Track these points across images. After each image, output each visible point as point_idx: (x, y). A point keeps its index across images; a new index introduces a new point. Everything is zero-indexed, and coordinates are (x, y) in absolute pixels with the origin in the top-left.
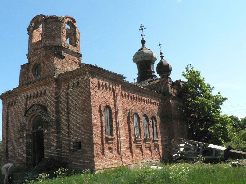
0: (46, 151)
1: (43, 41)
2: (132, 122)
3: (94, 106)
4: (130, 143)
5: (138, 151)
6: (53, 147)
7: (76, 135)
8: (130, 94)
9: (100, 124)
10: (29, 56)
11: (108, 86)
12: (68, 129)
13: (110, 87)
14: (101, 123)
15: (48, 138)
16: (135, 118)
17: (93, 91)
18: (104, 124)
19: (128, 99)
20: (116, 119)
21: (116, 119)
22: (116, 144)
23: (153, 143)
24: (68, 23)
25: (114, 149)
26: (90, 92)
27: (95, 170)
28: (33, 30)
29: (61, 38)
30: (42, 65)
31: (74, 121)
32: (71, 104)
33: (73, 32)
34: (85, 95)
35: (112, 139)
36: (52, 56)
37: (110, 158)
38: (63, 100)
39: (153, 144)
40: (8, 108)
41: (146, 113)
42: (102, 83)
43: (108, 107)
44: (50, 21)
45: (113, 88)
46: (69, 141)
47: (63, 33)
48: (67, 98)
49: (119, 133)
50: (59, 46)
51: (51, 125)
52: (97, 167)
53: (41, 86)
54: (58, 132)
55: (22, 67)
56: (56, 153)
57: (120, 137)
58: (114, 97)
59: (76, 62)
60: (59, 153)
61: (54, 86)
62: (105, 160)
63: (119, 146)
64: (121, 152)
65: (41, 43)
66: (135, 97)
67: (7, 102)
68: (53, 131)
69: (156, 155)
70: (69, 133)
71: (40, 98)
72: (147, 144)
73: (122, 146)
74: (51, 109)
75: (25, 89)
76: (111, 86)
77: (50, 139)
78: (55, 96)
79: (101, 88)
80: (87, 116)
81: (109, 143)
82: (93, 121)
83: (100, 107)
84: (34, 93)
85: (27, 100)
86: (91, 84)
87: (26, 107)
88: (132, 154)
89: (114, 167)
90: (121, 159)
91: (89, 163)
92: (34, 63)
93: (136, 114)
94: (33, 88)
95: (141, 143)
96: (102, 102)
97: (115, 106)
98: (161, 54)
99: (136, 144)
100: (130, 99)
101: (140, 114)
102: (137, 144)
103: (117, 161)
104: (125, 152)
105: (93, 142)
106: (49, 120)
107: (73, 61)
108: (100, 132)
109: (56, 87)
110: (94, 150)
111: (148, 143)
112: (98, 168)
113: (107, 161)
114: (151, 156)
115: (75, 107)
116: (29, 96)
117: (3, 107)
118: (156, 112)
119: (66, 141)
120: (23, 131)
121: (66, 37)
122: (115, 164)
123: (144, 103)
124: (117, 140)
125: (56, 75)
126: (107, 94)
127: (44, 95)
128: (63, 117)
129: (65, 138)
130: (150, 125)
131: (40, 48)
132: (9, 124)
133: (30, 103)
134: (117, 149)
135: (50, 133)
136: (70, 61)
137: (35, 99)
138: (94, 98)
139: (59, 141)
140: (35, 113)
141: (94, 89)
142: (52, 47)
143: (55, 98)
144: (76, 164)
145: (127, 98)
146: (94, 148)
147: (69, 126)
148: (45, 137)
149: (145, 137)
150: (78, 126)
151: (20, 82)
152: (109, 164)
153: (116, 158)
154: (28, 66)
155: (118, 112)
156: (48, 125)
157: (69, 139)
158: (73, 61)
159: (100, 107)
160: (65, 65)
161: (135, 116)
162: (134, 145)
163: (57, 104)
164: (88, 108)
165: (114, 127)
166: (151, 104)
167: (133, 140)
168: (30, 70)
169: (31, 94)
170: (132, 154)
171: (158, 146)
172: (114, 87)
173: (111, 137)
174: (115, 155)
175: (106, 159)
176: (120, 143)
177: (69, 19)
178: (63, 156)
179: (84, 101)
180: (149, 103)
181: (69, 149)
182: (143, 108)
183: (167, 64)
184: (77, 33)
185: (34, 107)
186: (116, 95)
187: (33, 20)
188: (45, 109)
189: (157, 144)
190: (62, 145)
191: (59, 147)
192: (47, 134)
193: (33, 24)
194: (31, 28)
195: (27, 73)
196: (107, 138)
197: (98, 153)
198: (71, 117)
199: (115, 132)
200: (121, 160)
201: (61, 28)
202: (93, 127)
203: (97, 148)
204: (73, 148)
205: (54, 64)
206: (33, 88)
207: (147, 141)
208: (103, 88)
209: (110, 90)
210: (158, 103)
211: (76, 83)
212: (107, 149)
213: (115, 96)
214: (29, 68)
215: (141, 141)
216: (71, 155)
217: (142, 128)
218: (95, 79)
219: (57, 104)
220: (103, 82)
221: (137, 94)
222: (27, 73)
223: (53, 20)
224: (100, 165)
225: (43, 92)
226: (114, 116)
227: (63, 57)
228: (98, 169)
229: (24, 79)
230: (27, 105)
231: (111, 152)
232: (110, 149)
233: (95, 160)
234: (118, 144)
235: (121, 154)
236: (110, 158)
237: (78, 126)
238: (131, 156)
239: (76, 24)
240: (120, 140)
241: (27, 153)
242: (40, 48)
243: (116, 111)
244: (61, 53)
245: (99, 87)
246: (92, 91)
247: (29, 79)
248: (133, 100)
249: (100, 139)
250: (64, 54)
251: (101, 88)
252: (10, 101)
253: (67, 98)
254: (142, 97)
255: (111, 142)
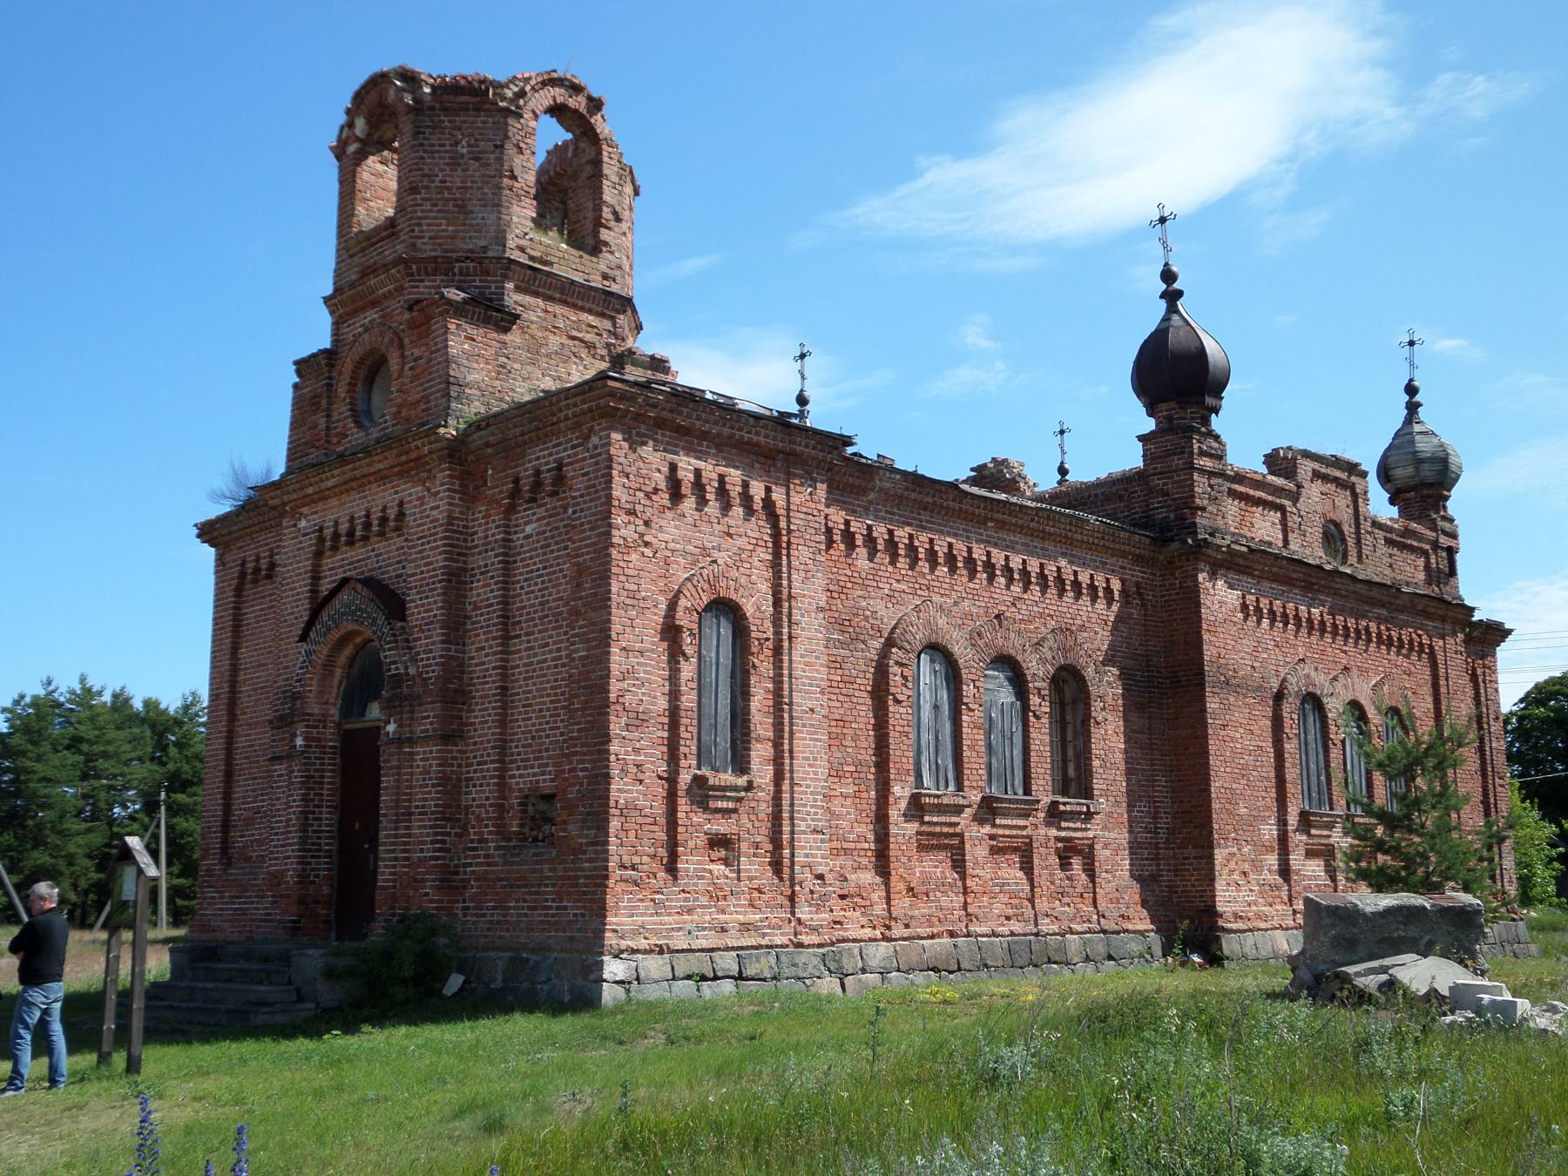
0: (387, 836)
1: (402, 225)
2: (899, 697)
3: (629, 601)
4: (881, 819)
5: (936, 867)
6: (420, 814)
7: (536, 759)
8: (902, 534)
9: (663, 703)
10: (342, 303)
11: (739, 489)
12: (503, 722)
13: (751, 498)
14: (674, 695)
15: (399, 767)
16: (927, 671)
17: (626, 518)
18: (688, 700)
19: (893, 562)
20: (777, 680)
21: (777, 680)
22: (762, 816)
23: (1048, 824)
24: (557, 111)
25: (744, 846)
26: (610, 525)
27: (602, 954)
28: (361, 156)
29: (499, 205)
30: (394, 363)
31: (532, 677)
32: (522, 588)
33: (588, 169)
34: (584, 539)
35: (736, 789)
36: (441, 314)
37: (717, 896)
38: (486, 561)
39: (1053, 832)
40: (239, 591)
41: (1012, 644)
42: (698, 473)
43: (725, 608)
44: (445, 109)
45: (774, 503)
46: (502, 786)
47: (514, 178)
48: (505, 554)
49: (792, 758)
50: (490, 254)
51: (419, 697)
52: (622, 938)
53: (382, 478)
54: (452, 734)
55: (304, 366)
56: (436, 850)
57: (792, 779)
58: (777, 554)
59: (590, 346)
60: (447, 850)
61: (442, 485)
62: (677, 901)
63: (786, 829)
64: (793, 863)
65: (393, 234)
66: (941, 549)
67: (234, 556)
68: (427, 731)
69: (1066, 900)
70: (503, 746)
71: (381, 546)
72: (1000, 832)
73: (804, 832)
74: (425, 607)
75: (310, 490)
76: (757, 490)
77: (412, 774)
78: (445, 538)
79: (689, 504)
80: (587, 657)
81: (717, 811)
82: (615, 687)
83: (672, 606)
84: (352, 519)
85: (319, 554)
86: (617, 480)
87: (314, 591)
88: (887, 884)
89: (731, 943)
90: (793, 906)
91: (583, 915)
92: (357, 352)
93: (937, 649)
94: (347, 487)
95: (954, 819)
96: (687, 579)
97: (777, 603)
98: (1168, 276)
99: (923, 823)
100: (903, 563)
101: (962, 652)
102: (924, 828)
103: (757, 917)
104: (820, 870)
105: (608, 798)
106: (412, 671)
107: (574, 338)
108: (665, 749)
109: (449, 490)
110: (607, 843)
111: (1004, 826)
112: (624, 944)
113: (690, 911)
114: (1031, 901)
115: (541, 604)
116: (328, 533)
117: (217, 584)
118: (1100, 639)
119: (488, 785)
120: (293, 722)
121: (535, 198)
122: (746, 927)
123: (1008, 587)
124: (774, 798)
125: (451, 421)
126: (729, 535)
127: (397, 529)
128: (482, 653)
129: (482, 771)
130: (1036, 716)
131: (386, 267)
132: (241, 677)
133: (336, 566)
134: (770, 847)
135: (411, 741)
136: (555, 341)
137: (359, 552)
138: (634, 557)
139: (451, 787)
140: (351, 627)
141: (639, 508)
142: (450, 261)
143: (445, 552)
144: (526, 915)
145: (883, 557)
146: (607, 835)
147: (504, 708)
148: (389, 758)
149: (995, 791)
150: (548, 710)
151: (295, 452)
152: (704, 929)
153: (756, 894)
154: (331, 366)
155: (790, 638)
156: (402, 700)
157: (502, 777)
158: (574, 338)
159: (672, 606)
160: (517, 366)
161: (932, 661)
162: (903, 830)
163: (456, 580)
164: (594, 610)
165: (761, 723)
166: (1062, 592)
167: (903, 805)
168: (342, 390)
169: (336, 523)
170: (887, 884)
171: (1091, 847)
172: (778, 496)
173: (728, 778)
174: (751, 879)
175: (686, 900)
176: (792, 812)
177: (558, 94)
178: (470, 865)
179: (580, 572)
180: (1044, 587)
181: (501, 831)
182: (998, 617)
183: (1193, 345)
184: (610, 170)
185: (344, 596)
186: (789, 543)
187: (358, 97)
188: (391, 602)
189: (1079, 835)
190: (467, 808)
191: (452, 812)
192: (399, 741)
193: (360, 125)
194: (352, 148)
195: (324, 403)
196: (699, 781)
197: (636, 860)
198: (520, 660)
199: (760, 754)
200: (793, 913)
201: (502, 147)
202: (612, 718)
203: (632, 834)
204: (521, 826)
205: (448, 362)
206: (347, 491)
207: (1006, 814)
208: (702, 502)
209: (749, 511)
210: (1116, 585)
211: (549, 471)
212: (701, 840)
213: (779, 546)
214: (334, 374)
215: (958, 810)
216: (506, 863)
217: (972, 736)
218: (647, 451)
219: (456, 580)
220: (701, 464)
221: (955, 535)
222: (324, 403)
223: (463, 98)
224: (639, 931)
225: (392, 513)
226: (763, 664)
227: (504, 320)
228: (622, 952)
229: (308, 437)
230: (319, 578)
231: (726, 862)
232: (721, 843)
233: (610, 901)
234: (776, 818)
235: (792, 878)
236: (717, 896)
237: (548, 710)
238: (878, 896)
239: (603, 125)
240: (792, 798)
241: (303, 841)
242: (386, 267)
243: (778, 633)
244: (501, 295)
245: (676, 495)
246: (619, 519)
247: (335, 440)
248: (924, 566)
249: (660, 790)
250: (513, 298)
251: (689, 504)
252: (250, 554)
253: (505, 554)
254: (994, 551)
255: (731, 805)
